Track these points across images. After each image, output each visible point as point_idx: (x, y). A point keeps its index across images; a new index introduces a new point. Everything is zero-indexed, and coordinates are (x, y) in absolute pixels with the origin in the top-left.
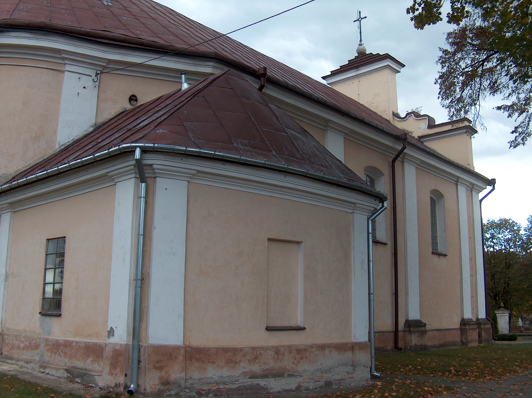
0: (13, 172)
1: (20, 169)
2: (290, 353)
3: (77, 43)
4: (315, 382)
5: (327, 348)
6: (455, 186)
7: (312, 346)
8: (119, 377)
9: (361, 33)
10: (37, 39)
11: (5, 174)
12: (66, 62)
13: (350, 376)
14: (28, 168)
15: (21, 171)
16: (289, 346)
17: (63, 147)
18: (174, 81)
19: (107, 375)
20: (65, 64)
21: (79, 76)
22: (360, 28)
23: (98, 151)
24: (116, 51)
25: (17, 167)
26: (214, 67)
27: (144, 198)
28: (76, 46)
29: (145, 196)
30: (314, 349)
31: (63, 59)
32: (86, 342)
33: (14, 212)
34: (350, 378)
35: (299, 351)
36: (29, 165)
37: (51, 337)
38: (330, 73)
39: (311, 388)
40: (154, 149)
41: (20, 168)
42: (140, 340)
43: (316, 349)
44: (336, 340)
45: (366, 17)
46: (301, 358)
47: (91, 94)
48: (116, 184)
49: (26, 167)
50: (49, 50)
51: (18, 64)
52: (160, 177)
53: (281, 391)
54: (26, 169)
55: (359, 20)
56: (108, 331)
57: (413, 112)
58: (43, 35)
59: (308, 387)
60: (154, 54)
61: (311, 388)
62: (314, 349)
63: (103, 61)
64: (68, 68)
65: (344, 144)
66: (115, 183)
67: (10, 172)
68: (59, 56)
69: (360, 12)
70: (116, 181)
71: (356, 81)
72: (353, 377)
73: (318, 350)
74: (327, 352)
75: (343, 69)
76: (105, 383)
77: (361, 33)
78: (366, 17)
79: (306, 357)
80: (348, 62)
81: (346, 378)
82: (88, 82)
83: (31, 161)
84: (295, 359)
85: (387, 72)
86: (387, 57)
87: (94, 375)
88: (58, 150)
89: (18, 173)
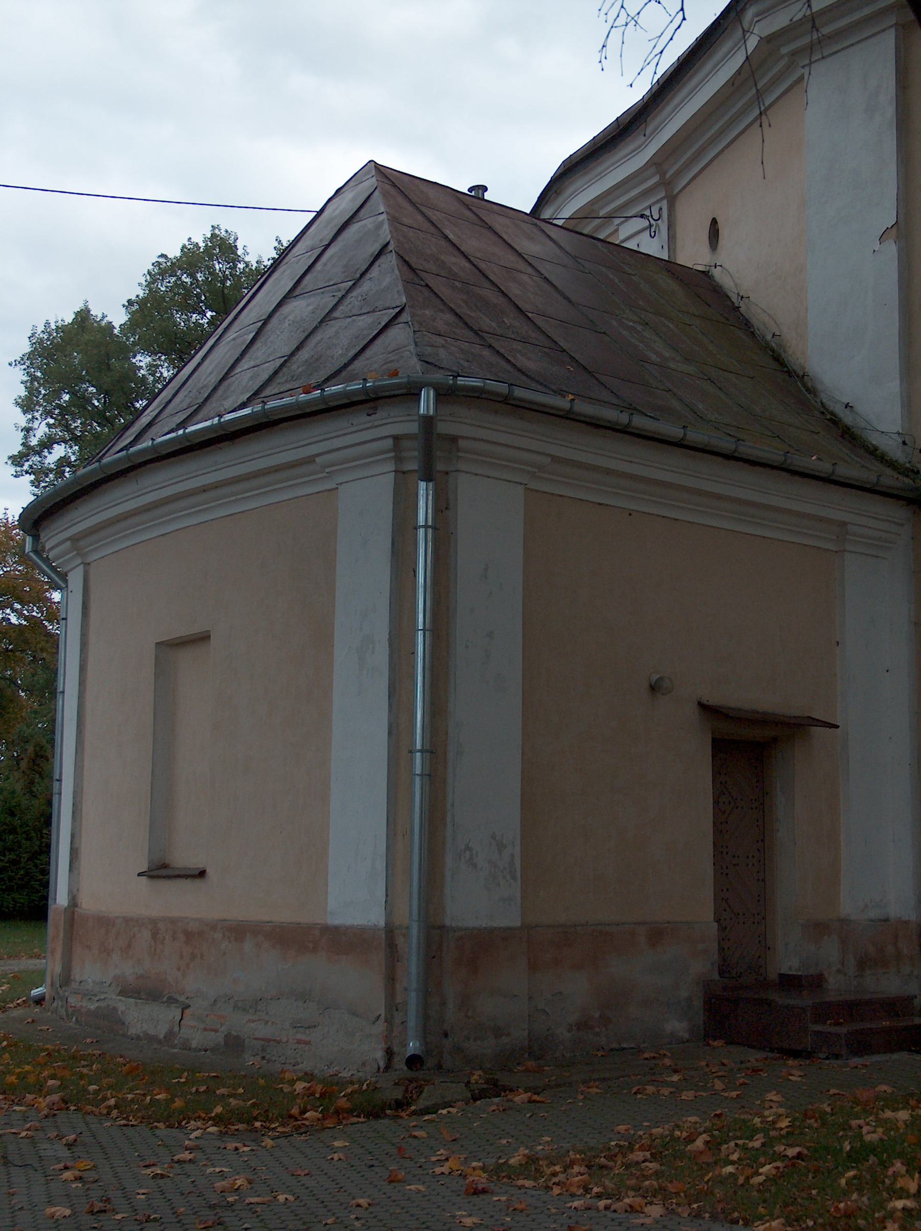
2: (174, 940)
3: (599, 169)
4: (205, 1029)
5: (248, 935)
6: (394, 470)
7: (213, 926)
13: (299, 1036)
16: (173, 921)
23: (329, 383)
27: (430, 531)
28: (601, 176)
29: (434, 519)
30: (218, 935)
34: (299, 1042)
35: (189, 936)
39: (194, 1044)
42: (162, 865)
43: (224, 935)
44: (284, 915)
46: (193, 957)
48: (337, 488)
53: (141, 1034)
59: (188, 1040)
61: (194, 1044)
62: (218, 935)
65: (713, 757)
66: (335, 486)
72: (308, 1043)
73: (229, 938)
74: (248, 945)
79: (202, 957)
81: (284, 1040)
84: (181, 957)
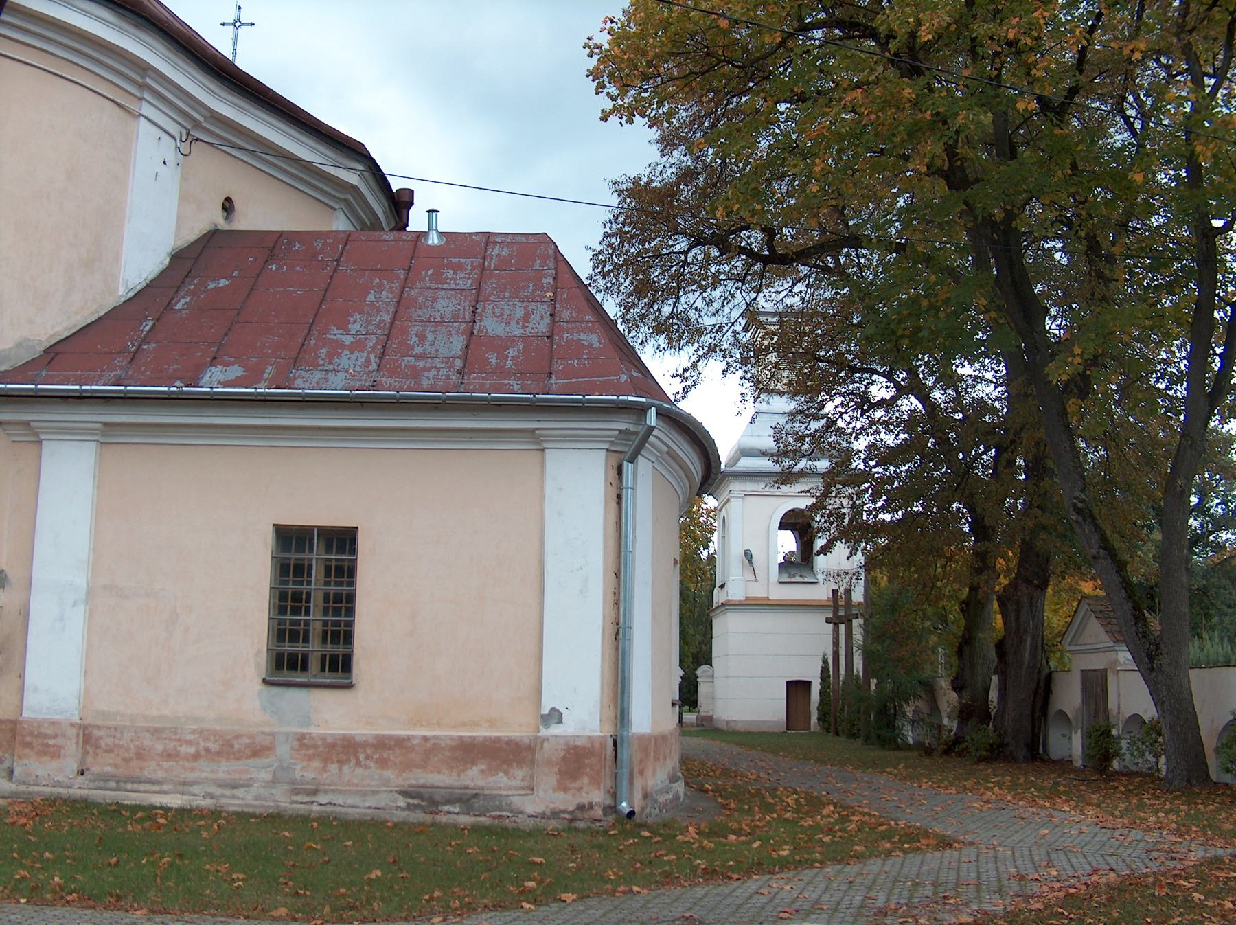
0: (46, 337)
1: (58, 334)
3: (181, 63)
8: (588, 793)
10: (121, 30)
11: (29, 340)
12: (147, 96)
14: (73, 331)
15: (59, 338)
17: (131, 294)
18: (310, 195)
19: (551, 792)
20: (141, 99)
21: (160, 133)
24: (230, 97)
25: (53, 327)
28: (175, 67)
31: (142, 86)
32: (461, 737)
33: (101, 443)
36: (75, 326)
37: (313, 730)
40: (617, 405)
41: (58, 329)
45: (224, 24)
47: (171, 178)
49: (70, 328)
50: (125, 58)
51: (60, 73)
52: (646, 458)
54: (69, 334)
56: (542, 716)
58: (137, 26)
60: (277, 119)
63: (203, 111)
64: (146, 110)
67: (38, 335)
68: (138, 79)
69: (240, 8)
70: (545, 445)
76: (547, 807)
78: (224, 24)
82: (168, 148)
83: (79, 317)
87: (508, 796)
88: (123, 300)
89: (53, 342)
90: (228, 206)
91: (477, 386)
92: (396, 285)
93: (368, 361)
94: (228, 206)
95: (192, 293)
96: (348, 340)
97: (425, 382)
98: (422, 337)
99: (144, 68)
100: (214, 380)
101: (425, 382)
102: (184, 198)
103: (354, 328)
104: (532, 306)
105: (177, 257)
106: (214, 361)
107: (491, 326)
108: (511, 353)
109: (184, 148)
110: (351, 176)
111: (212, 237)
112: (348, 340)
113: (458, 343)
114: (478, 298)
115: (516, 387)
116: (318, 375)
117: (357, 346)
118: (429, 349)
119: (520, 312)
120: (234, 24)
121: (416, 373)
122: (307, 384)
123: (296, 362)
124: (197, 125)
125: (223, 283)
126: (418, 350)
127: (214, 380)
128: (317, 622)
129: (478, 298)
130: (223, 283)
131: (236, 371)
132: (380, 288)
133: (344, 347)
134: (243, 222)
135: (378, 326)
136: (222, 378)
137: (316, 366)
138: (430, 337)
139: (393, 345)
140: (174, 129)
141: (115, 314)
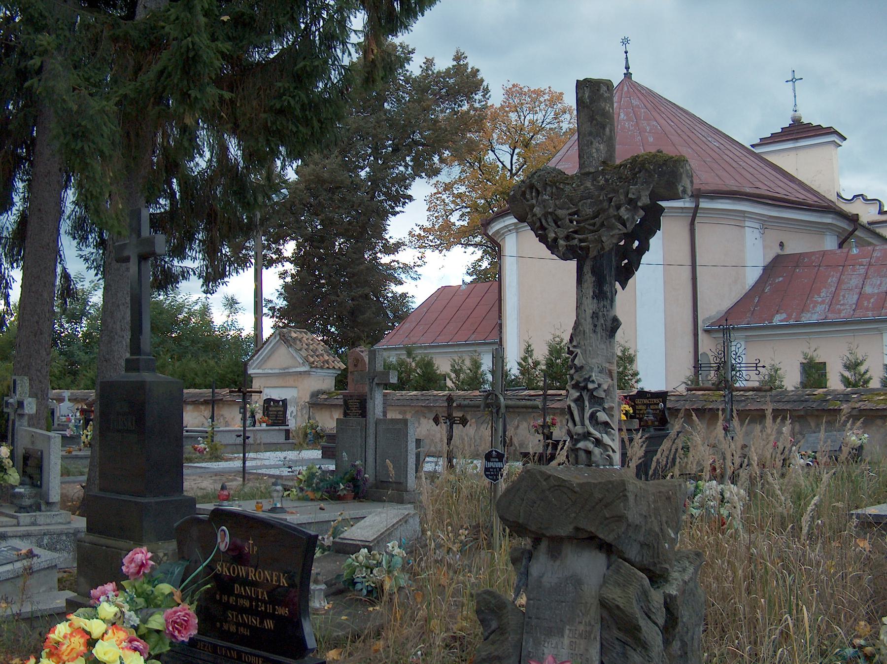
9: (795, 96)
22: (794, 91)
26: (833, 218)
38: (758, 141)
47: (759, 243)
55: (793, 80)
57: (862, 195)
64: (747, 224)
71: (792, 155)
75: (775, 139)
77: (795, 96)
80: (780, 131)
82: (757, 233)
85: (832, 147)
86: (830, 131)
90: (782, 245)
91: (859, 315)
92: (838, 274)
93: (825, 308)
94: (782, 245)
95: (770, 284)
96: (820, 300)
97: (842, 315)
98: (844, 296)
99: (744, 212)
100: (777, 320)
101: (842, 315)
102: (764, 247)
103: (823, 294)
104: (884, 279)
105: (765, 269)
106: (777, 312)
107: (868, 289)
108: (872, 300)
109: (762, 231)
110: (828, 219)
111: (778, 259)
112: (820, 300)
113: (856, 297)
114: (866, 277)
115: (870, 315)
116: (809, 315)
117: (823, 302)
118: (846, 301)
119: (879, 282)
120: (792, 80)
121: (840, 311)
122: (805, 319)
123: (802, 311)
124: (765, 221)
125: (781, 279)
126: (842, 302)
127: (777, 320)
128: (42, 523)
129: (866, 277)
130: (781, 279)
131: (784, 316)
132: (833, 276)
133: (818, 303)
134: (788, 251)
135: (830, 293)
136: (780, 319)
137: (809, 311)
138: (847, 296)
139: (834, 301)
140: (757, 226)
141: (746, 295)
